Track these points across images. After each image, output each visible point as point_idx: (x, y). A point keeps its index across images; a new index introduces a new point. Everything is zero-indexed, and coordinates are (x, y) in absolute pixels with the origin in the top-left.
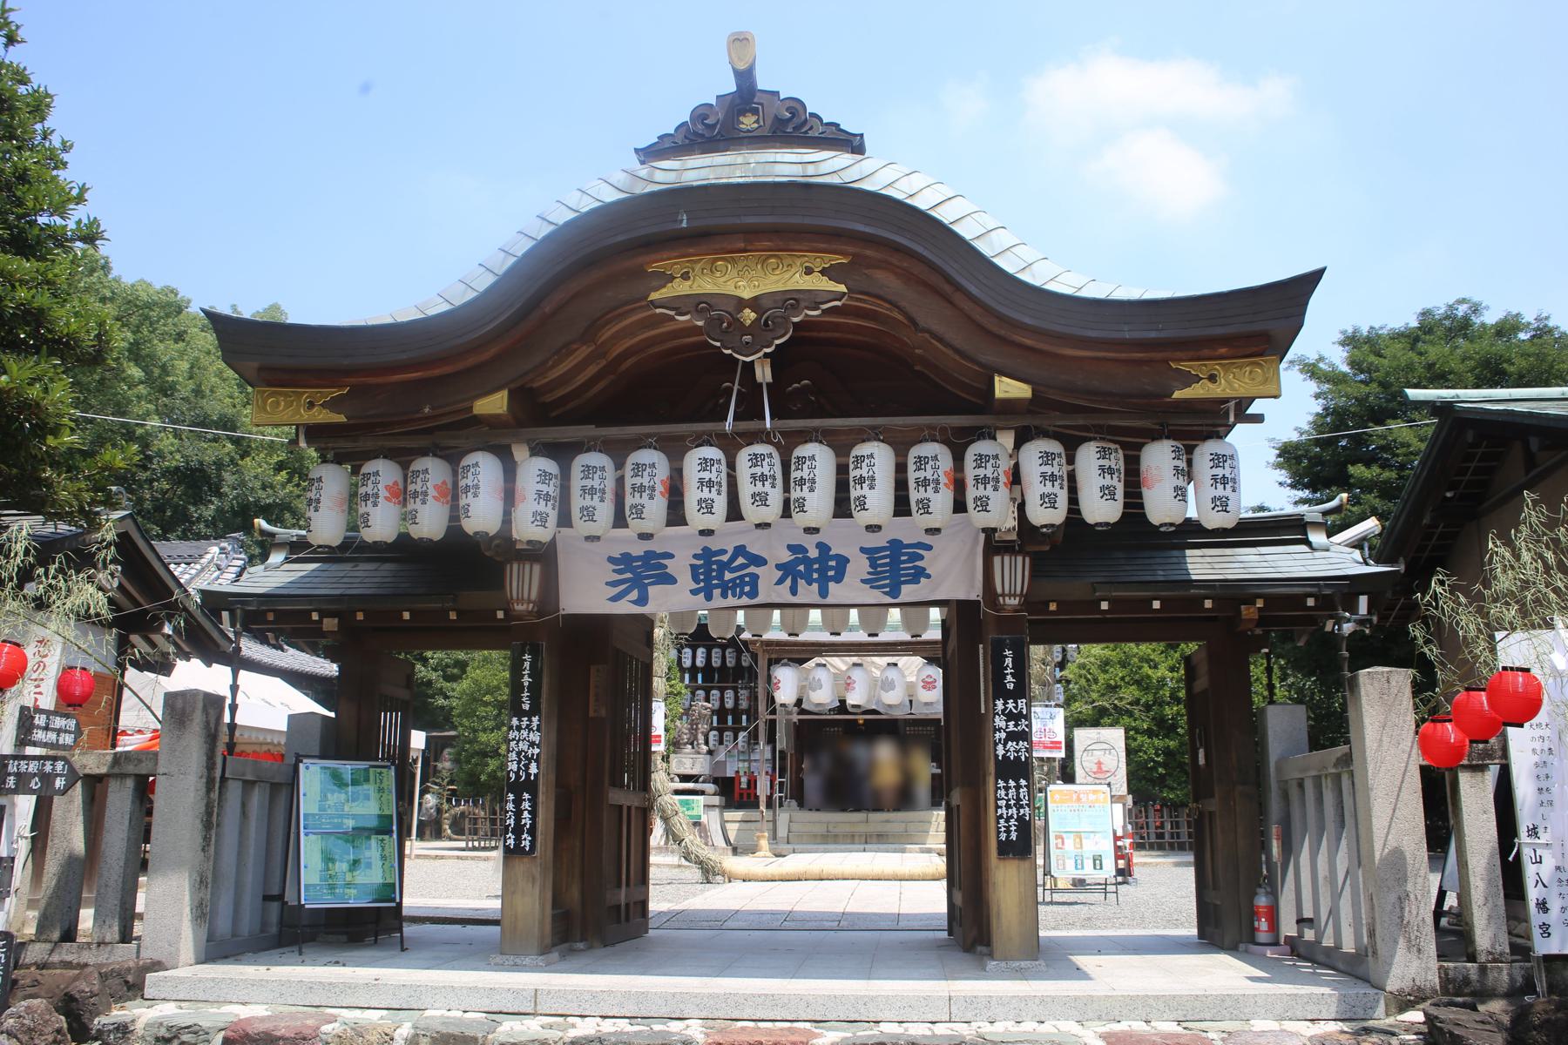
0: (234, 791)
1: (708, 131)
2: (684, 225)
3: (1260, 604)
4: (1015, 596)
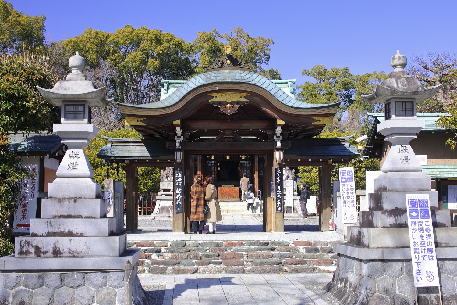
2: (218, 89)
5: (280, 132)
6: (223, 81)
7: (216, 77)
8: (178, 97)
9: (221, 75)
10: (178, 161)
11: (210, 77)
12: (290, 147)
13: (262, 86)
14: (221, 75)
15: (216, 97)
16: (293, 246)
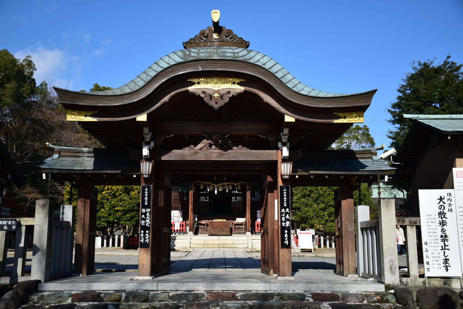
0: (55, 228)
1: (202, 39)
2: (200, 70)
3: (356, 177)
4: (287, 175)
5: (287, 137)
6: (209, 58)
7: (198, 53)
8: (143, 82)
9: (206, 50)
10: (146, 176)
11: (190, 53)
12: (300, 157)
13: (263, 66)
14: (206, 50)
15: (199, 83)
16: (311, 300)
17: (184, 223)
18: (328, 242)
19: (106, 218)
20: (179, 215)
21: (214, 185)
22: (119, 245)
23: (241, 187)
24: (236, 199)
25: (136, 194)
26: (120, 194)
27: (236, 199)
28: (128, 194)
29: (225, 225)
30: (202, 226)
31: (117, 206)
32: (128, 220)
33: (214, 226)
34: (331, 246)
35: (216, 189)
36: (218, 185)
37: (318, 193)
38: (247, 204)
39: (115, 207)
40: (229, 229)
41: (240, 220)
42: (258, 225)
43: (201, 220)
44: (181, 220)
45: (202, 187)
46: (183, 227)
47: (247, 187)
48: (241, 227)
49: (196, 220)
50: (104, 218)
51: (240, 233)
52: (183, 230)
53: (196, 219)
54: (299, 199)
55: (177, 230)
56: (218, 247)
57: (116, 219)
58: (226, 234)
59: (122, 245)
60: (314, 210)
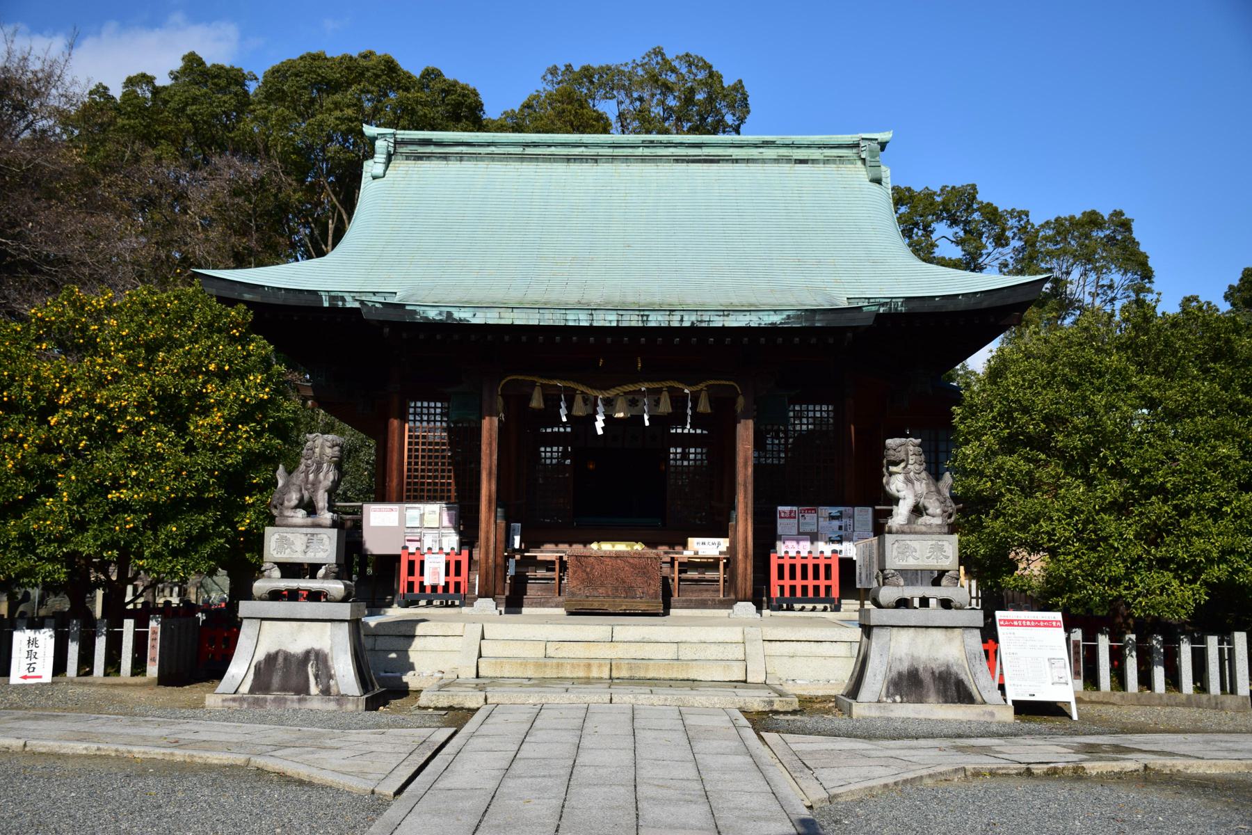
17: (464, 558)
18: (1132, 665)
19: (62, 540)
20: (446, 522)
21: (592, 393)
22: (139, 666)
23: (712, 402)
24: (685, 456)
25: (218, 427)
26: (136, 429)
27: (685, 456)
28: (182, 430)
29: (640, 567)
30: (541, 573)
31: (116, 486)
32: (175, 553)
33: (589, 571)
34: (1146, 680)
35: (600, 409)
36: (611, 393)
37: (1089, 430)
38: (740, 478)
39: (108, 490)
40: (657, 587)
41: (705, 547)
42: (781, 567)
43: (537, 545)
44: (451, 540)
45: (537, 402)
46: (458, 573)
47: (741, 401)
48: (709, 575)
49: (517, 546)
50: (49, 541)
51: (703, 605)
52: (457, 585)
53: (517, 539)
54: (990, 455)
55: (434, 588)
56: (606, 675)
57: (113, 544)
58: (642, 607)
59: (153, 670)
60: (1074, 511)
